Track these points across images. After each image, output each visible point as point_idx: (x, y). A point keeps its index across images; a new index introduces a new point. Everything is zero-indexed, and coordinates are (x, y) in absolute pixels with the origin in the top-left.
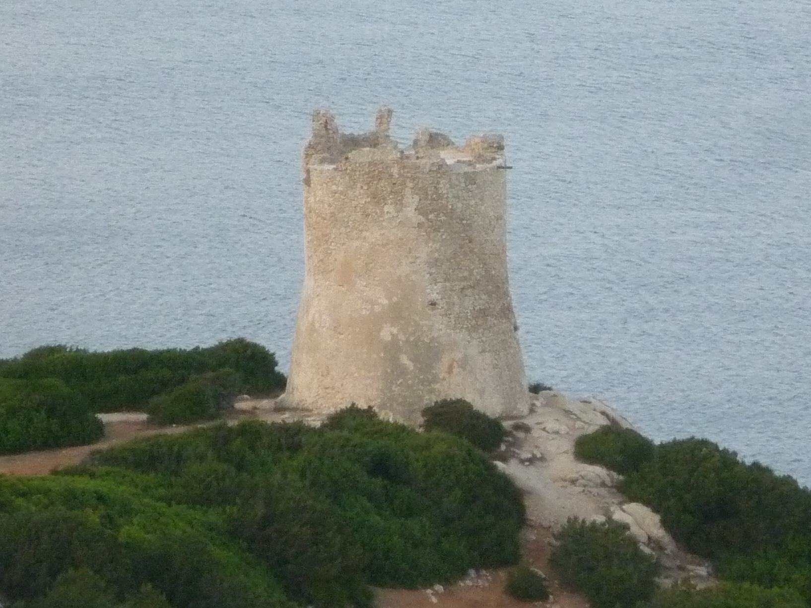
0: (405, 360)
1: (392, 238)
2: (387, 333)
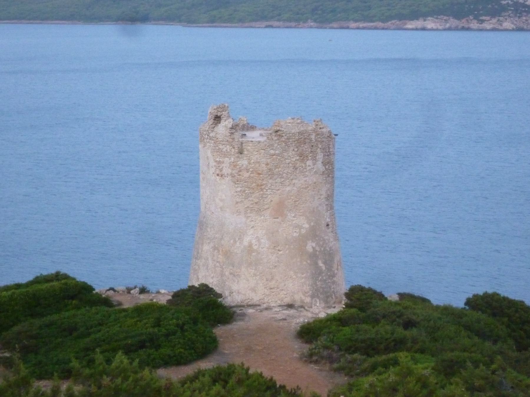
0: (321, 264)
1: (310, 183)
2: (310, 246)
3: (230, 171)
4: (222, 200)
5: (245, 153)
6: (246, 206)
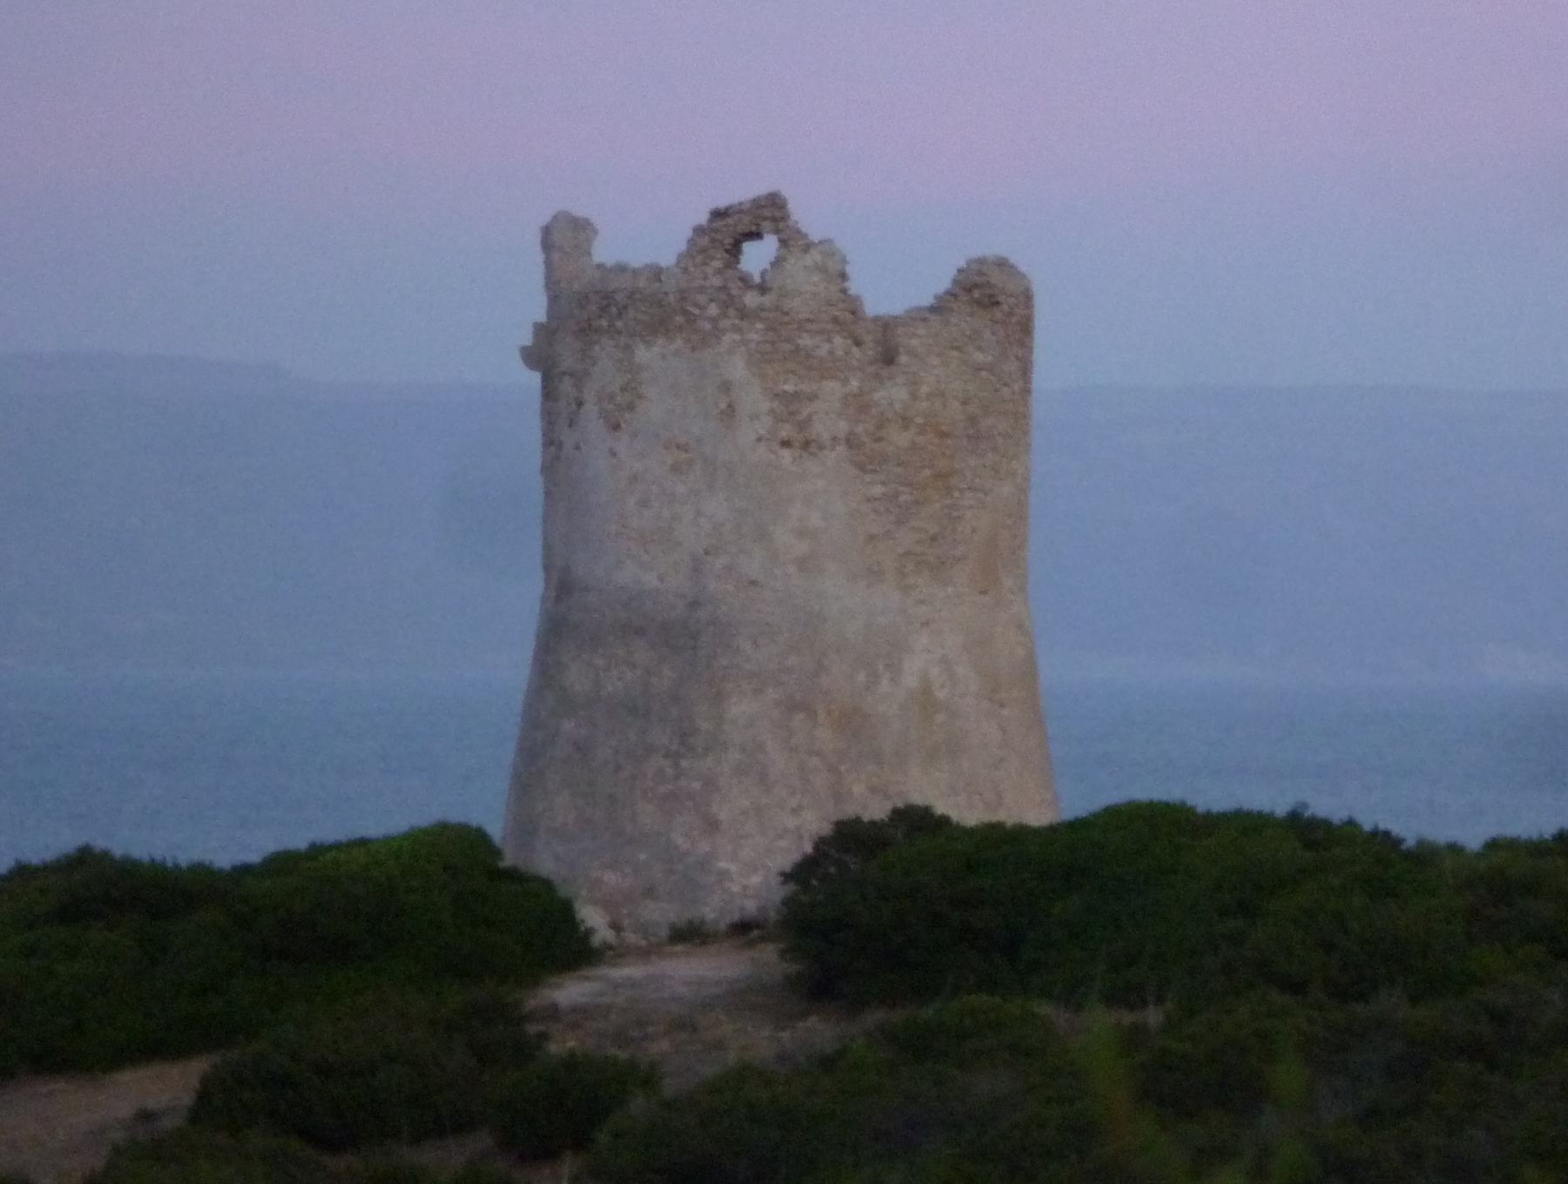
3: (843, 427)
4: (802, 533)
5: (903, 359)
6: (900, 550)
